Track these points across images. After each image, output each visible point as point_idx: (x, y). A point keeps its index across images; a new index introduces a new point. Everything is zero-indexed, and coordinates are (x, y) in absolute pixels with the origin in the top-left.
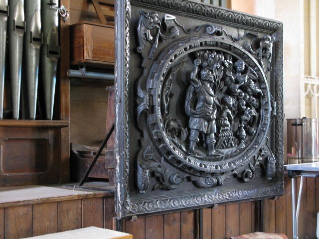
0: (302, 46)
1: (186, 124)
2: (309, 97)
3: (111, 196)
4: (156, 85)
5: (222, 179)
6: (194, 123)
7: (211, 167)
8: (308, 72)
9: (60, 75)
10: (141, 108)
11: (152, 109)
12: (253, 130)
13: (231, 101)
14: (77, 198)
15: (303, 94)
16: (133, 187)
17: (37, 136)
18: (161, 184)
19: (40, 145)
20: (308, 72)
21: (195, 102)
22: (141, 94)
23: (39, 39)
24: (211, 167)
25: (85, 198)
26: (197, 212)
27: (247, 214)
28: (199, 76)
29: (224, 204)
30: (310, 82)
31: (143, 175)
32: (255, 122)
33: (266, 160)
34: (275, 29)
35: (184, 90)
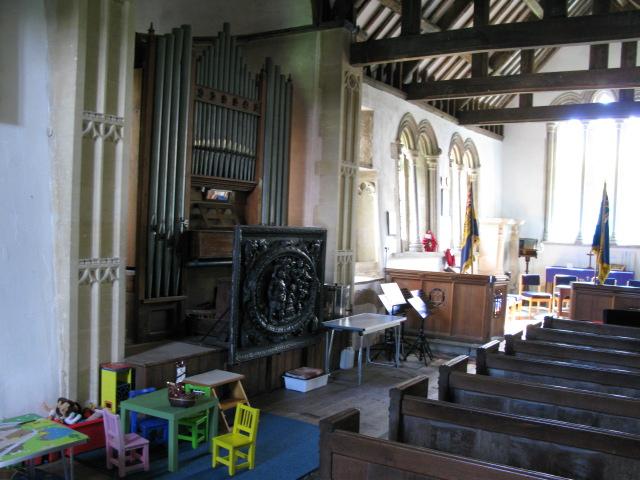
0: (338, 229)
1: (268, 305)
2: (340, 265)
3: (227, 350)
4: (252, 284)
5: (286, 337)
6: (273, 304)
7: (280, 330)
8: (341, 247)
9: (182, 266)
10: (246, 299)
11: (251, 300)
12: (305, 304)
13: (294, 287)
14: (484, 438)
15: (336, 264)
16: (239, 347)
17: (167, 307)
18: (253, 343)
19: (169, 312)
20: (341, 247)
21: (273, 292)
22: (246, 291)
23: (171, 242)
24: (280, 330)
25: (213, 352)
26: (269, 359)
27: (297, 356)
28: (276, 275)
29: (286, 352)
30: (342, 254)
31: (246, 337)
32: (307, 297)
33: (312, 321)
34: (321, 234)
35: (267, 280)
